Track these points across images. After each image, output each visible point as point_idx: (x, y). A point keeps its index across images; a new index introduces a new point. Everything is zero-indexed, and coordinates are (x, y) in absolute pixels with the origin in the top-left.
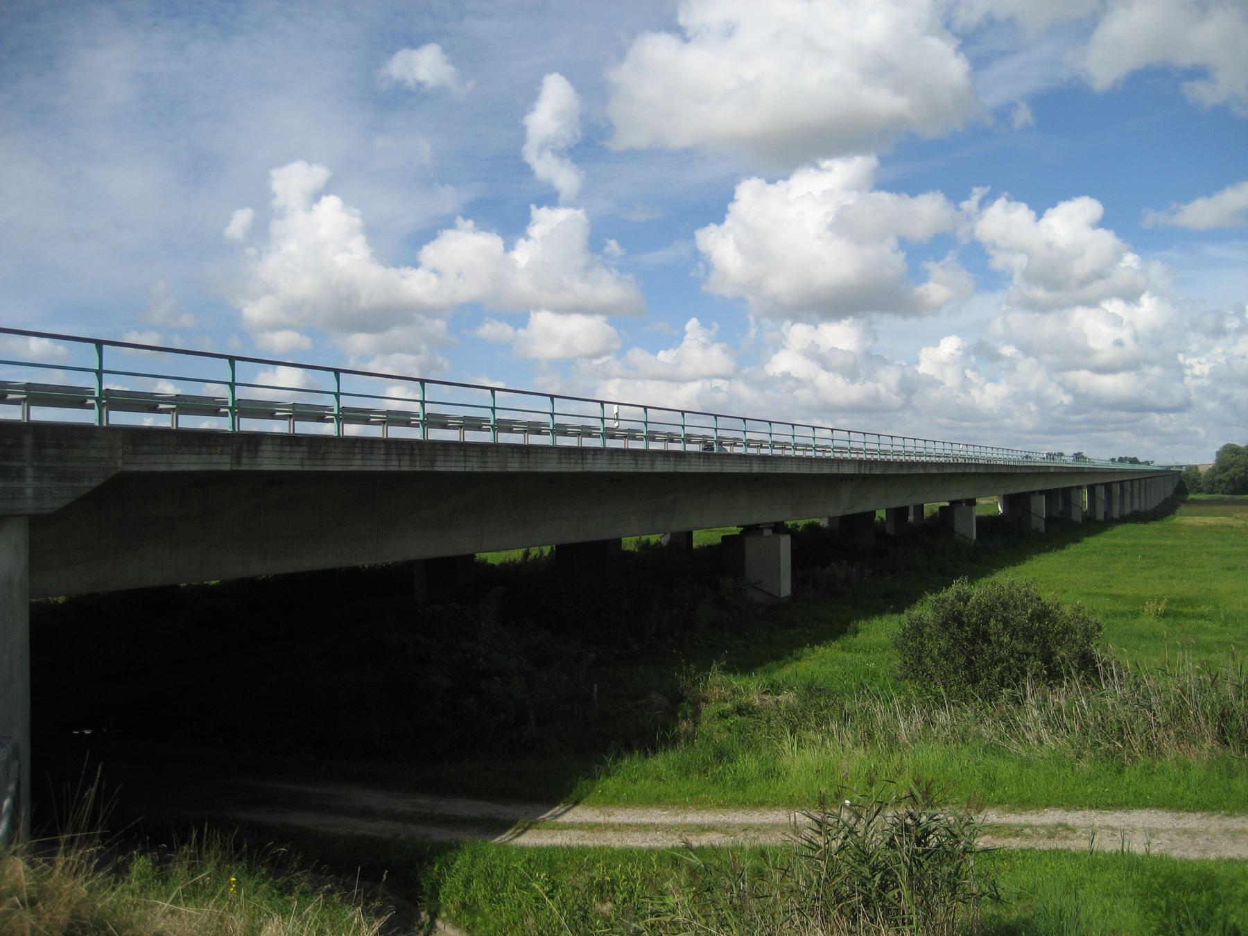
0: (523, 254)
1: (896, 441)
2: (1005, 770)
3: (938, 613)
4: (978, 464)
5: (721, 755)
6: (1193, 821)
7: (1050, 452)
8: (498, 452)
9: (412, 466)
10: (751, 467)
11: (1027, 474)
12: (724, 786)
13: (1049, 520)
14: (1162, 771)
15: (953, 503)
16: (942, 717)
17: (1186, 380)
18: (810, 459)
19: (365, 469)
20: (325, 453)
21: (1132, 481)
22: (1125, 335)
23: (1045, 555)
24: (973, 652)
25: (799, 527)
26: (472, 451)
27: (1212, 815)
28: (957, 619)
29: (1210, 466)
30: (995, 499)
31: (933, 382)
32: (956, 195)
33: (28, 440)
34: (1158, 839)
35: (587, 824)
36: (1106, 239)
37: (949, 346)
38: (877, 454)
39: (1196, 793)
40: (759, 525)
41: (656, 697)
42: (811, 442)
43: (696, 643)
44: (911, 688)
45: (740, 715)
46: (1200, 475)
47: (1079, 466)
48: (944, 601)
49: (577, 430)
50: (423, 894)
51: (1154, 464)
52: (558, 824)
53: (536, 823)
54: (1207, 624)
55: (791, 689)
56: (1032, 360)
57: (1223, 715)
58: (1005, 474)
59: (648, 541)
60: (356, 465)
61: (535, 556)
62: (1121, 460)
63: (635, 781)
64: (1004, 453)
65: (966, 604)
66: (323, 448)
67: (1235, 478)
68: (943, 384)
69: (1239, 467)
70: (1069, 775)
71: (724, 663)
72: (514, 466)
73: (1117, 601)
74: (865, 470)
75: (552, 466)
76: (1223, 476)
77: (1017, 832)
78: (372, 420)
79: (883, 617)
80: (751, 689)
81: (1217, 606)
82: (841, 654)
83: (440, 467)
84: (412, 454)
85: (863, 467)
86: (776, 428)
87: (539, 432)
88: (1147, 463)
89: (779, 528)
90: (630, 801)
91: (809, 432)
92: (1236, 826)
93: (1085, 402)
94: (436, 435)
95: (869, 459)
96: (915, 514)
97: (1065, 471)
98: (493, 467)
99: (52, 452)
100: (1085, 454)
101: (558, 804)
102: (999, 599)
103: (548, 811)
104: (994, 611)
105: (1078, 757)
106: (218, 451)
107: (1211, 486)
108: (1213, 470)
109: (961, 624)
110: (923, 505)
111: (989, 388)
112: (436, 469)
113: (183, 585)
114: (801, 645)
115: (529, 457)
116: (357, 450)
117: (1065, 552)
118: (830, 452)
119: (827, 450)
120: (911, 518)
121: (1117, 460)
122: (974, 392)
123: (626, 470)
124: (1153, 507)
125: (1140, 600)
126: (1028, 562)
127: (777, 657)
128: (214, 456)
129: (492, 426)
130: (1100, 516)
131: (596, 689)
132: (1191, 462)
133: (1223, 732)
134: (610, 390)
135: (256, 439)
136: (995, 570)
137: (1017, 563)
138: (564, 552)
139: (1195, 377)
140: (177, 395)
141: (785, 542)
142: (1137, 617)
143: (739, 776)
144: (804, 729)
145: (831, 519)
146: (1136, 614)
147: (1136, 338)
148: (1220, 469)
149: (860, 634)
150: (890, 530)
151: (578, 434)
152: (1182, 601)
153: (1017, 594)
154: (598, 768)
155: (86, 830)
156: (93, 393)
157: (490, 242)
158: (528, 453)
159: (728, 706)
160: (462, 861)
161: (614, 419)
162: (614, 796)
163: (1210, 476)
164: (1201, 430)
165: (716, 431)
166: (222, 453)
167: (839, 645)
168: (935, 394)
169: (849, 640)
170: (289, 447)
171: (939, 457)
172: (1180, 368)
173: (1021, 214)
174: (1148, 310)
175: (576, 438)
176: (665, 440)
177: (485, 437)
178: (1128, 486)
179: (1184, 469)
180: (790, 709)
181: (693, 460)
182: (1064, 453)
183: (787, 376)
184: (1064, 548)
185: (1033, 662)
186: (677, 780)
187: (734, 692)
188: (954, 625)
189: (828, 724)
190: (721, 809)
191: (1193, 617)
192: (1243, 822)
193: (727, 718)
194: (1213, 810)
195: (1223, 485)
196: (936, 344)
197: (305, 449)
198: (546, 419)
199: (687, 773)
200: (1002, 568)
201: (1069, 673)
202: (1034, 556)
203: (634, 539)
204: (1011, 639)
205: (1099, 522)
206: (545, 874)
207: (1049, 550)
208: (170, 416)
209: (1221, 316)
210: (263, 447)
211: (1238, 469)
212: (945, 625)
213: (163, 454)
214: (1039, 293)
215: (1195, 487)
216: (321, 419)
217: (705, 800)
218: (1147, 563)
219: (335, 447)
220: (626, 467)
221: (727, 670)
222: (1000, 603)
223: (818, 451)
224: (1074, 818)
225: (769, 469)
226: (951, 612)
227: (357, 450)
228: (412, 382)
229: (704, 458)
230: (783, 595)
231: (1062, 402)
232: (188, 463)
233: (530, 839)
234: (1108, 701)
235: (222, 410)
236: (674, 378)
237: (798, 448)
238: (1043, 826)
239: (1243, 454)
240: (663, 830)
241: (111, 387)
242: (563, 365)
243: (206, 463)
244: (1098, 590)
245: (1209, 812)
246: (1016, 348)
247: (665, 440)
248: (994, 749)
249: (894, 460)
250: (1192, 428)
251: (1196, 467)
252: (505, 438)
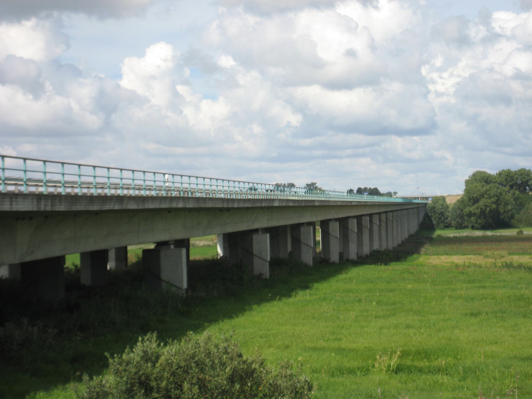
1: (99, 172)
3: (121, 378)
7: (279, 183)
13: (275, 263)
15: (161, 245)
17: (431, 97)
21: (371, 215)
23: (267, 304)
29: (459, 198)
30: (214, 237)
38: (60, 187)
46: (448, 207)
47: (321, 199)
48: (128, 363)
51: (398, 195)
56: (255, 74)
58: (221, 210)
62: (360, 191)
65: (154, 366)
67: (486, 209)
68: (147, 100)
69: (490, 198)
73: (346, 356)
76: (472, 209)
79: (67, 386)
81: (455, 358)
88: (389, 194)
100: (318, 185)
102: (193, 357)
104: (188, 373)
107: (460, 220)
108: (461, 201)
110: (125, 248)
111: (205, 104)
117: (291, 300)
121: (355, 191)
122: (188, 111)
126: (247, 313)
130: (335, 257)
132: (438, 193)
139: (439, 95)
142: (367, 374)
146: (366, 371)
147: (373, 47)
148: (470, 200)
150: (86, 280)
153: (214, 350)
163: (459, 208)
164: (448, 155)
172: (423, 82)
178: (366, 221)
179: (430, 201)
182: (295, 184)
184: (290, 296)
188: (140, 392)
191: (430, 372)
196: (141, 54)
202: (255, 307)
205: (334, 264)
207: (272, 299)
211: (490, 201)
215: (443, 222)
218: (382, 310)
222: (195, 362)
226: (137, 376)
231: (289, 123)
239: (494, 182)
244: (324, 344)
246: (235, 60)
249: (83, 194)
251: (443, 198)
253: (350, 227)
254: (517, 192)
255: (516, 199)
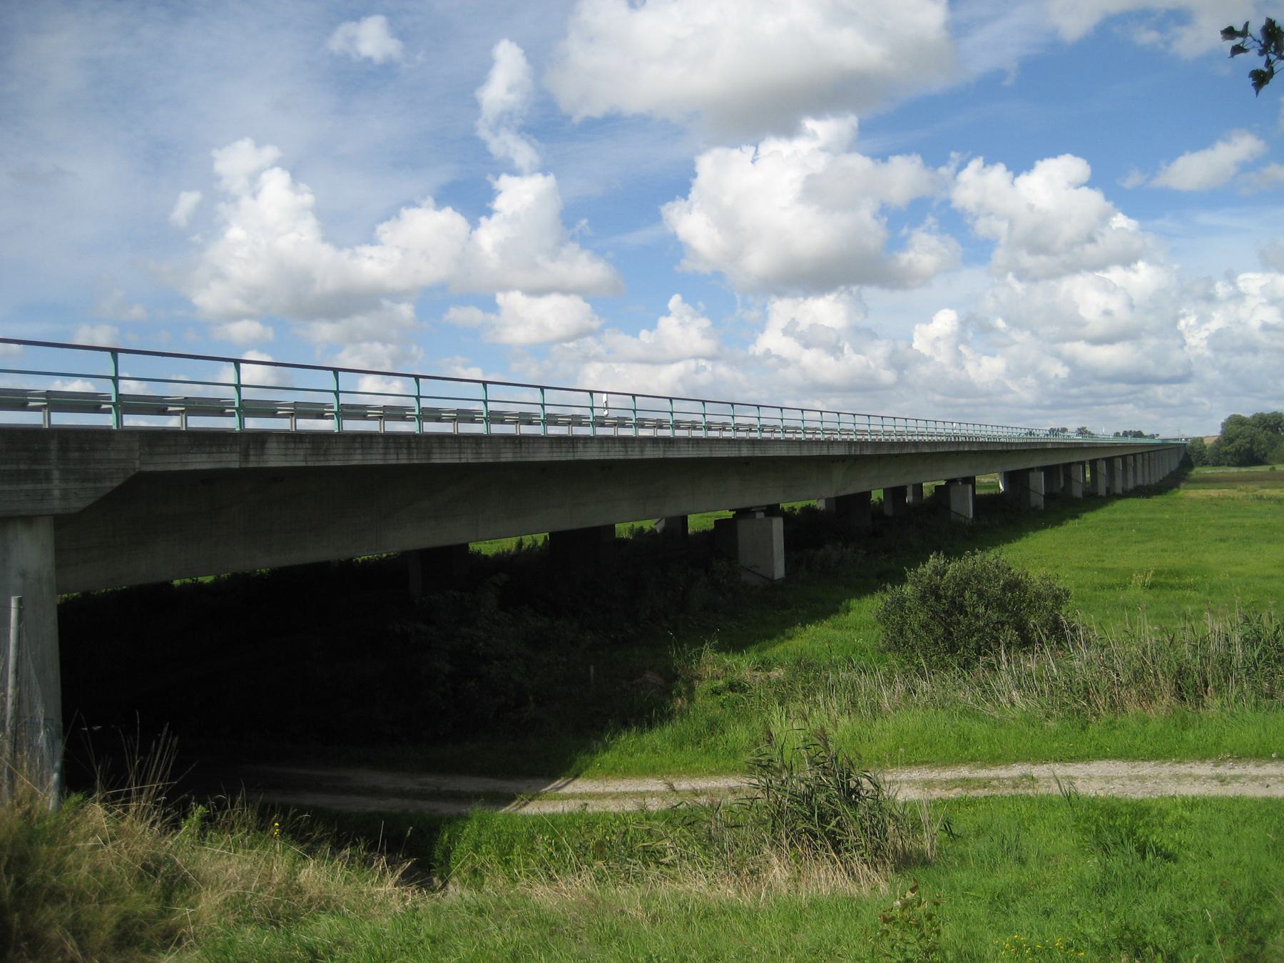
0: (489, 235)
2: (979, 730)
4: (959, 442)
5: (713, 725)
6: (1146, 768)
7: (1054, 428)
8: (491, 443)
9: (409, 459)
10: (740, 451)
11: (1025, 450)
12: (716, 755)
13: (1049, 497)
14: (1123, 725)
16: (924, 685)
18: (799, 442)
19: (365, 463)
20: (327, 449)
21: (1134, 455)
22: (1115, 304)
24: (950, 625)
25: (796, 510)
26: (467, 443)
27: (1165, 763)
28: (935, 592)
29: (1216, 438)
31: (921, 359)
32: (933, 157)
33: (54, 445)
34: (1112, 784)
35: (586, 794)
36: (1093, 200)
37: (945, 321)
39: (1151, 745)
40: (751, 508)
41: (651, 677)
42: (799, 424)
43: (690, 626)
44: (893, 659)
45: (733, 691)
46: (1205, 447)
48: (922, 575)
49: (452, 415)
50: (435, 861)
52: (558, 795)
53: (539, 795)
54: (1188, 593)
55: (782, 665)
57: (1180, 673)
59: (642, 529)
60: (357, 459)
61: (529, 546)
62: (1125, 434)
63: (631, 755)
64: (975, 429)
66: (325, 444)
69: (1244, 439)
70: (1038, 733)
71: (716, 641)
72: (507, 456)
74: (855, 451)
75: (543, 455)
76: (1227, 448)
77: (985, 784)
78: (369, 415)
80: (743, 666)
82: (831, 632)
83: (437, 459)
84: (409, 448)
85: (853, 449)
86: (764, 412)
87: (530, 423)
88: (1152, 437)
89: (772, 511)
90: (626, 773)
91: (798, 415)
92: (1184, 772)
93: (1082, 375)
94: (431, 427)
95: (846, 439)
96: (914, 494)
97: (1062, 446)
98: (487, 458)
99: (75, 455)
100: (1088, 429)
101: (559, 778)
103: (549, 784)
105: (1046, 717)
106: (228, 449)
108: (1218, 442)
109: (938, 598)
112: (433, 461)
113: (177, 582)
114: (792, 624)
115: (521, 448)
116: (357, 445)
118: (780, 432)
119: (817, 432)
120: (909, 499)
121: (1121, 434)
122: (970, 368)
123: (616, 457)
124: (1157, 481)
125: (1129, 573)
126: (1024, 539)
127: (769, 637)
128: (223, 455)
129: (485, 419)
130: (1102, 491)
131: (592, 671)
132: (1197, 435)
133: (1180, 689)
134: (592, 376)
135: (261, 438)
136: (990, 548)
137: (1013, 541)
138: (557, 538)
140: (186, 398)
141: (778, 524)
143: (730, 746)
144: (792, 701)
145: (828, 500)
146: (1125, 587)
147: (1131, 306)
149: (851, 613)
150: (888, 511)
151: (454, 420)
152: (1170, 572)
154: (597, 745)
155: (304, 819)
156: (110, 398)
157: (447, 220)
158: (520, 443)
159: (721, 682)
160: (471, 829)
161: (604, 408)
162: (612, 769)
163: (1216, 448)
165: (704, 417)
166: (231, 452)
167: (830, 624)
168: (925, 370)
169: (841, 619)
170: (293, 444)
171: (932, 436)
173: (998, 174)
174: (1143, 277)
175: (514, 426)
176: (655, 427)
177: (478, 429)
178: (1130, 460)
180: (779, 682)
181: (682, 446)
182: (1067, 427)
183: (768, 354)
185: (1008, 631)
186: (672, 752)
187: (726, 670)
189: (815, 695)
190: (713, 776)
192: (1191, 767)
193: (719, 694)
194: (1165, 758)
195: (1229, 457)
196: (928, 320)
197: (308, 446)
198: (537, 409)
199: (681, 745)
200: (997, 545)
201: (1040, 641)
202: (1031, 533)
203: (629, 525)
204: (986, 609)
206: (548, 837)
207: (1045, 527)
208: (179, 417)
209: (1210, 282)
210: (268, 445)
212: (923, 599)
213: (176, 454)
214: (1027, 261)
215: (1201, 460)
216: (321, 416)
217: (698, 769)
219: (336, 443)
220: (616, 454)
221: (720, 649)
223: (807, 433)
224: (1040, 771)
225: (758, 453)
227: (357, 445)
228: (193, 360)
229: (693, 444)
230: (776, 577)
232: (200, 462)
233: (532, 809)
234: (1076, 663)
235: (104, 406)
236: (654, 360)
237: (787, 431)
238: (1008, 779)
240: (658, 797)
241: (549, 412)
242: (539, 350)
243: (217, 462)
245: (1162, 760)
247: (655, 427)
248: (968, 713)
249: (858, 439)
250: (1195, 399)
251: (1202, 439)
252: (497, 429)
253: (1116, 466)
254: (1270, 433)
255: (1269, 439)
